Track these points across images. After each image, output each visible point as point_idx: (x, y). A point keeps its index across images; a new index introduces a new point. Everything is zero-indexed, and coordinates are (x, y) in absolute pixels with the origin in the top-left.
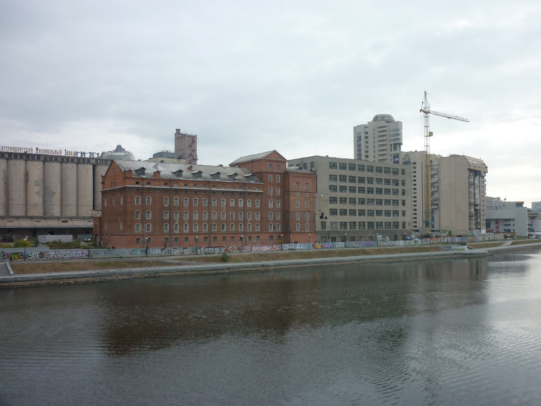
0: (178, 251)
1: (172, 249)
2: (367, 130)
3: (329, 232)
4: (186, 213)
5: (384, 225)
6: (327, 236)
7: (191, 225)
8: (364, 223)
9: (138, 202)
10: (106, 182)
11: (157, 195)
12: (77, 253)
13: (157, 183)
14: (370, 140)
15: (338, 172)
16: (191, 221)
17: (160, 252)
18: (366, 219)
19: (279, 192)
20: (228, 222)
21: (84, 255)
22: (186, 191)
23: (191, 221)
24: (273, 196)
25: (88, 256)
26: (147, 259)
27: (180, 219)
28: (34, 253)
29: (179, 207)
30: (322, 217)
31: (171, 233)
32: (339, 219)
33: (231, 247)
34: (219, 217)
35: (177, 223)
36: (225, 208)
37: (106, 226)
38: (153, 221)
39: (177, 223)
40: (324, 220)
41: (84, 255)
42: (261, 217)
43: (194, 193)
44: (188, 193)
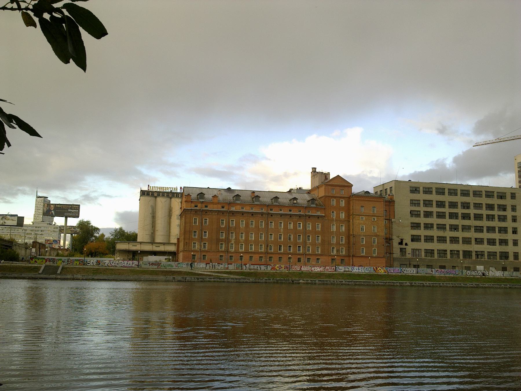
0: (223, 266)
1: (216, 264)
3: (410, 260)
5: (486, 254)
6: (408, 263)
7: (247, 245)
8: (458, 251)
9: (195, 222)
12: (128, 263)
15: (421, 197)
16: (247, 241)
17: (204, 266)
18: (460, 247)
19: (343, 216)
21: (134, 265)
22: (243, 213)
23: (247, 241)
24: (336, 220)
25: (138, 265)
26: (192, 271)
27: (236, 239)
28: (92, 261)
30: (401, 243)
31: (227, 251)
32: (423, 246)
33: (278, 266)
36: (282, 230)
39: (233, 242)
40: (404, 246)
41: (134, 265)
43: (251, 215)
44: (245, 215)
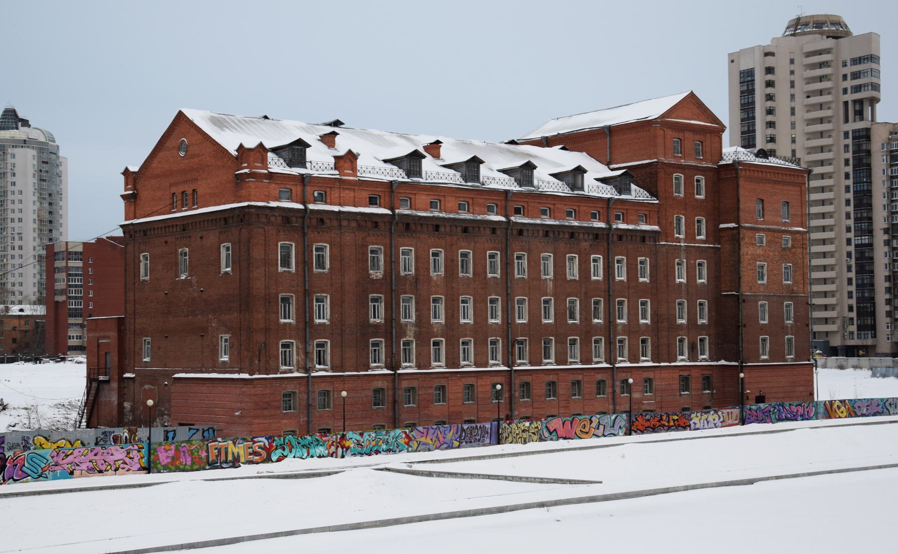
2: (770, 61)
4: (435, 301)
10: (144, 194)
11: (348, 238)
13: (348, 194)
14: (782, 91)
16: (452, 329)
20: (560, 332)
29: (416, 278)
34: (534, 317)
35: (410, 337)
36: (550, 285)
37: (146, 347)
38: (336, 330)
39: (410, 337)
42: (656, 316)
44: (442, 229)
